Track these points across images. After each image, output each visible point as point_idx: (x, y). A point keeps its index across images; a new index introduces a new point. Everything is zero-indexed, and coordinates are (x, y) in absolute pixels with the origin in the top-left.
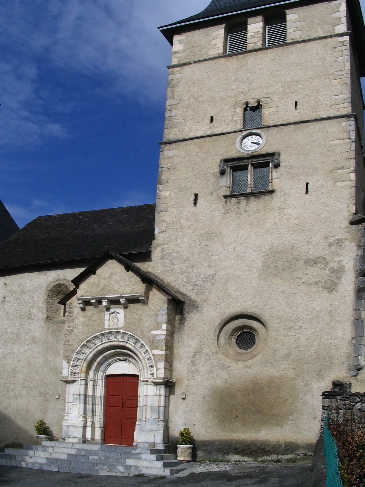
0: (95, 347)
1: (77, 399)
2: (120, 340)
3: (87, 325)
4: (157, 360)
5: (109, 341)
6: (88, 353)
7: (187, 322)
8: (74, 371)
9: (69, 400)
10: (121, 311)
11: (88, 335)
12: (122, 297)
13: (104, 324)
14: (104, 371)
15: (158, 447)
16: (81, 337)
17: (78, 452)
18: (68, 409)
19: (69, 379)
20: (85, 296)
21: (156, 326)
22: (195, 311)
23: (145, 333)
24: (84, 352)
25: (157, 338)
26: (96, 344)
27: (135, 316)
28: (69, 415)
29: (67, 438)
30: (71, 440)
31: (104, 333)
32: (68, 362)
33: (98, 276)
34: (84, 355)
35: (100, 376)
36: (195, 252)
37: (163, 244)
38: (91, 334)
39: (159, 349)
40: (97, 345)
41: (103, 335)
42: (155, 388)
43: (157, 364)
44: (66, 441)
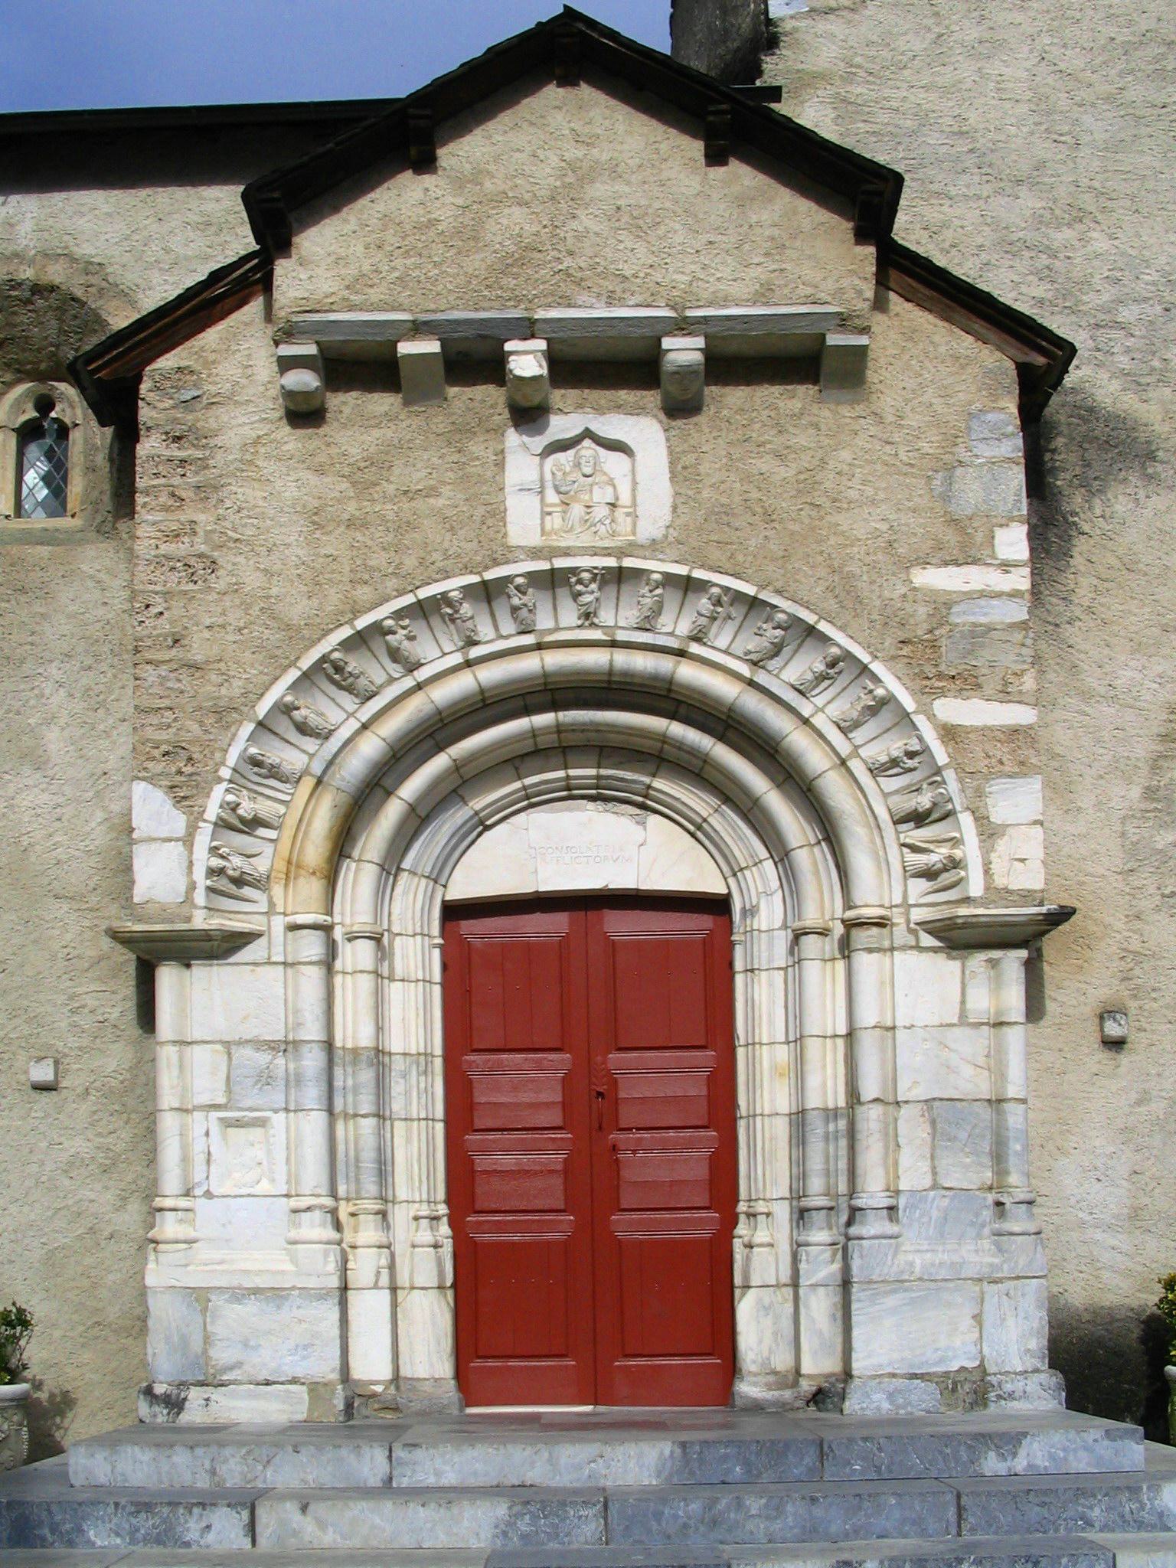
0: (408, 682)
1: (265, 1078)
2: (621, 636)
3: (350, 524)
4: (981, 765)
5: (529, 640)
6: (345, 733)
7: (1081, 547)
8: (237, 861)
9: (185, 1090)
10: (642, 429)
11: (363, 593)
12: (683, 326)
13: (498, 514)
14: (438, 877)
15: (1011, 1396)
16: (298, 608)
17: (524, 1525)
18: (185, 1160)
19: (200, 921)
20: (352, 308)
21: (951, 537)
22: (1133, 479)
23: (862, 584)
24: (314, 720)
25: (961, 616)
26: (412, 667)
27: (765, 464)
28: (201, 1204)
29: (195, 1395)
30: (237, 1407)
31: (508, 579)
32: (185, 793)
33: (459, 183)
34: (310, 744)
35: (413, 908)
36: (1085, 139)
37: (849, 78)
38: (392, 583)
39: (989, 690)
40: (422, 674)
41: (488, 593)
42: (949, 968)
43: (980, 793)
44: (193, 1414)
